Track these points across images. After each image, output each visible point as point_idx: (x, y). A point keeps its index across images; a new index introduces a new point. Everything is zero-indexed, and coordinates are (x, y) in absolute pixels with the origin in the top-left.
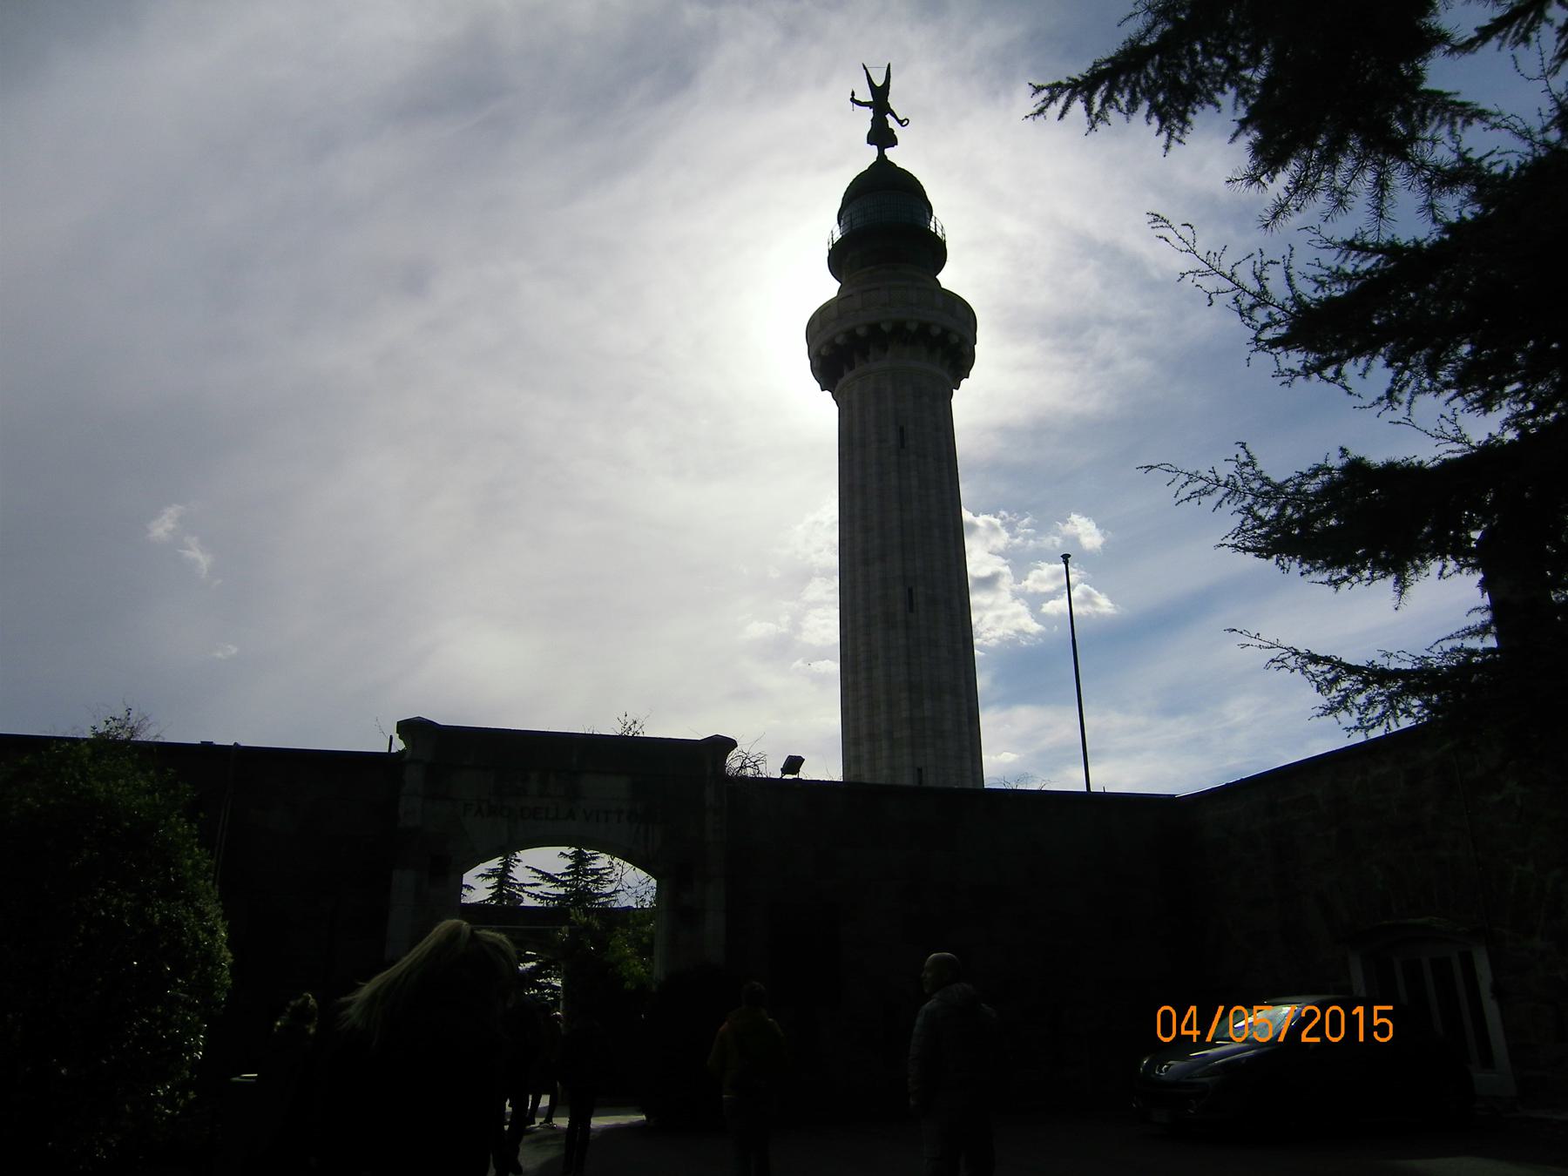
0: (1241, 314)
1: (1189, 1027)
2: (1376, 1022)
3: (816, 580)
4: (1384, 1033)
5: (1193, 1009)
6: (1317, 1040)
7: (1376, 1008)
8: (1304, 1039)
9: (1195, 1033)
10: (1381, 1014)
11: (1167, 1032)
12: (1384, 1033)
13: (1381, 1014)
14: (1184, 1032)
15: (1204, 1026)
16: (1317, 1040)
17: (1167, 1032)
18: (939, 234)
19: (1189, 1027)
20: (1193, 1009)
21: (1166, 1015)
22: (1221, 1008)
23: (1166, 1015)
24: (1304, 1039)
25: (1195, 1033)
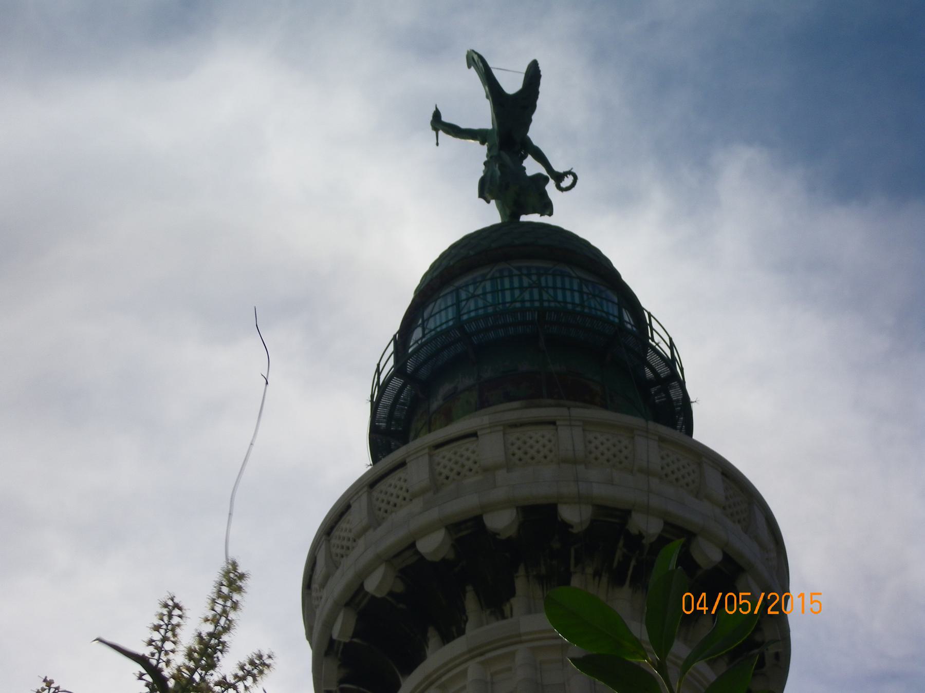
0: (177, 606)
1: (702, 605)
2: (741, 603)
3: (239, 571)
4: (745, 609)
5: (704, 594)
6: (777, 613)
7: (741, 594)
8: (769, 612)
9: (705, 609)
10: (744, 598)
11: (688, 608)
12: (745, 609)
13: (744, 598)
14: (698, 608)
15: (710, 605)
16: (777, 613)
17: (688, 608)
18: (391, 349)
19: (702, 605)
20: (704, 594)
21: (689, 598)
22: (720, 594)
23: (689, 598)
24: (769, 612)
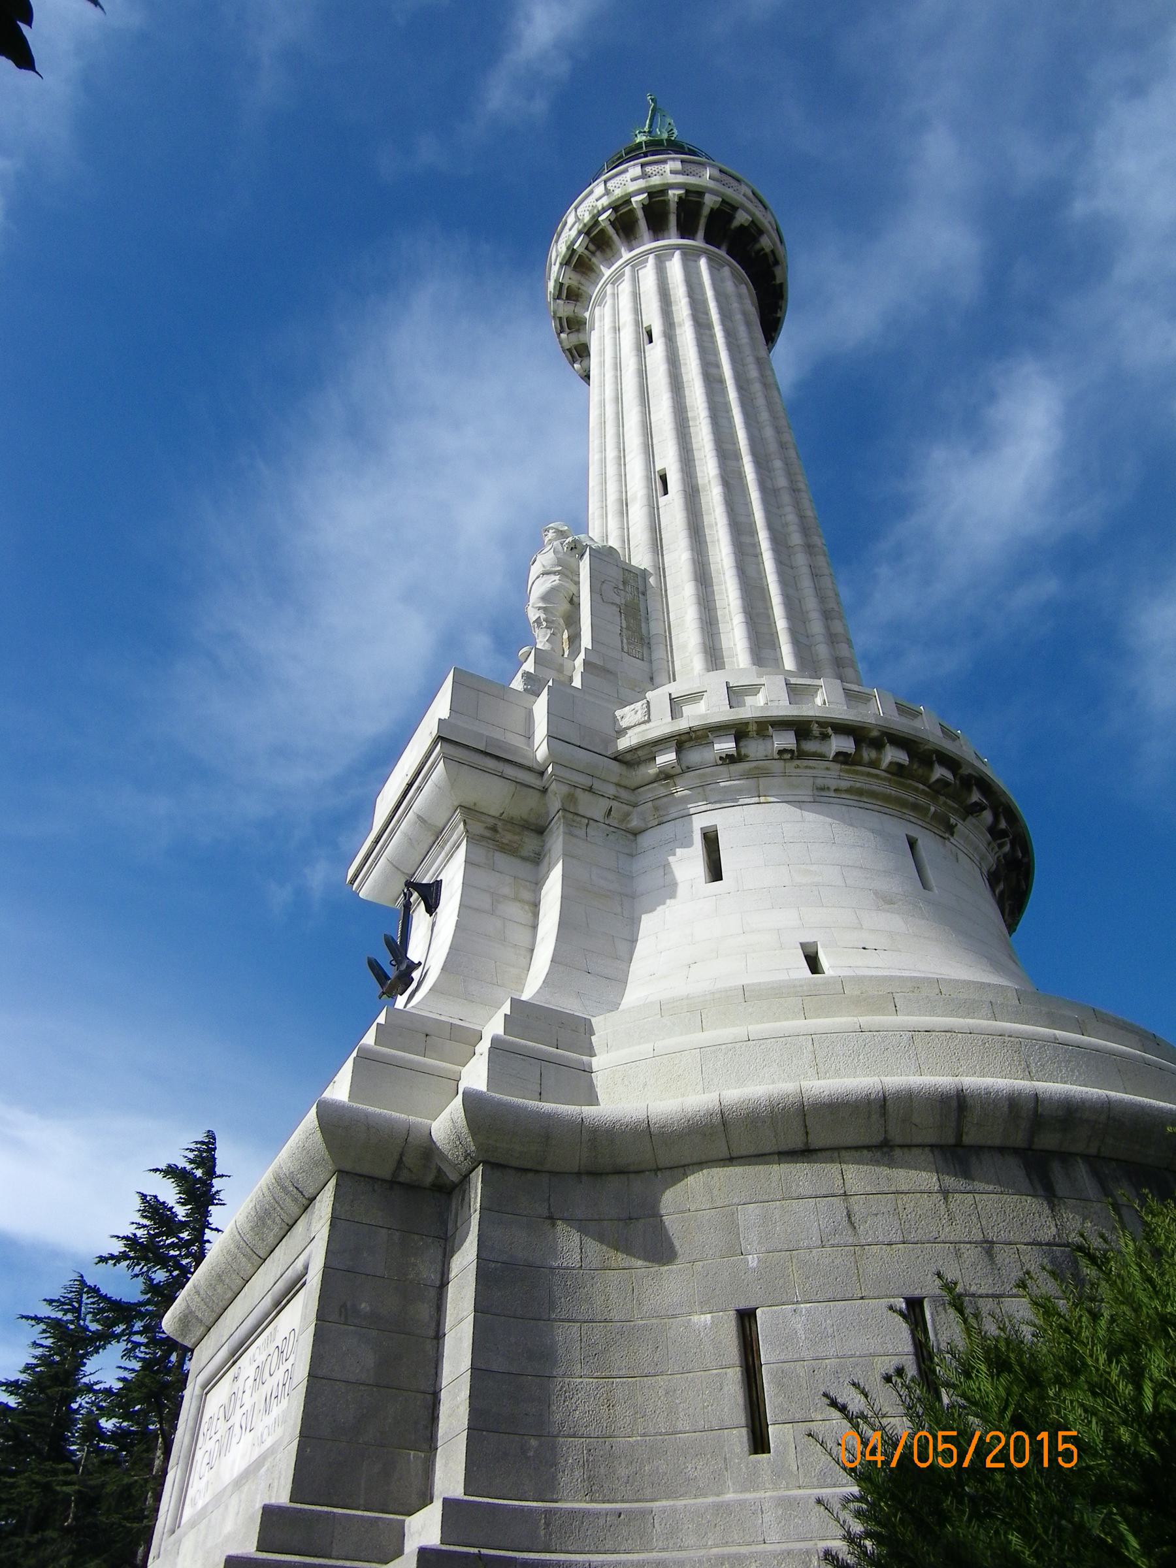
2: (941, 1447)
6: (1002, 1465)
7: (1061, 1434)
8: (989, 1465)
10: (946, 1439)
16: (1002, 1465)
25: (879, 1458)
